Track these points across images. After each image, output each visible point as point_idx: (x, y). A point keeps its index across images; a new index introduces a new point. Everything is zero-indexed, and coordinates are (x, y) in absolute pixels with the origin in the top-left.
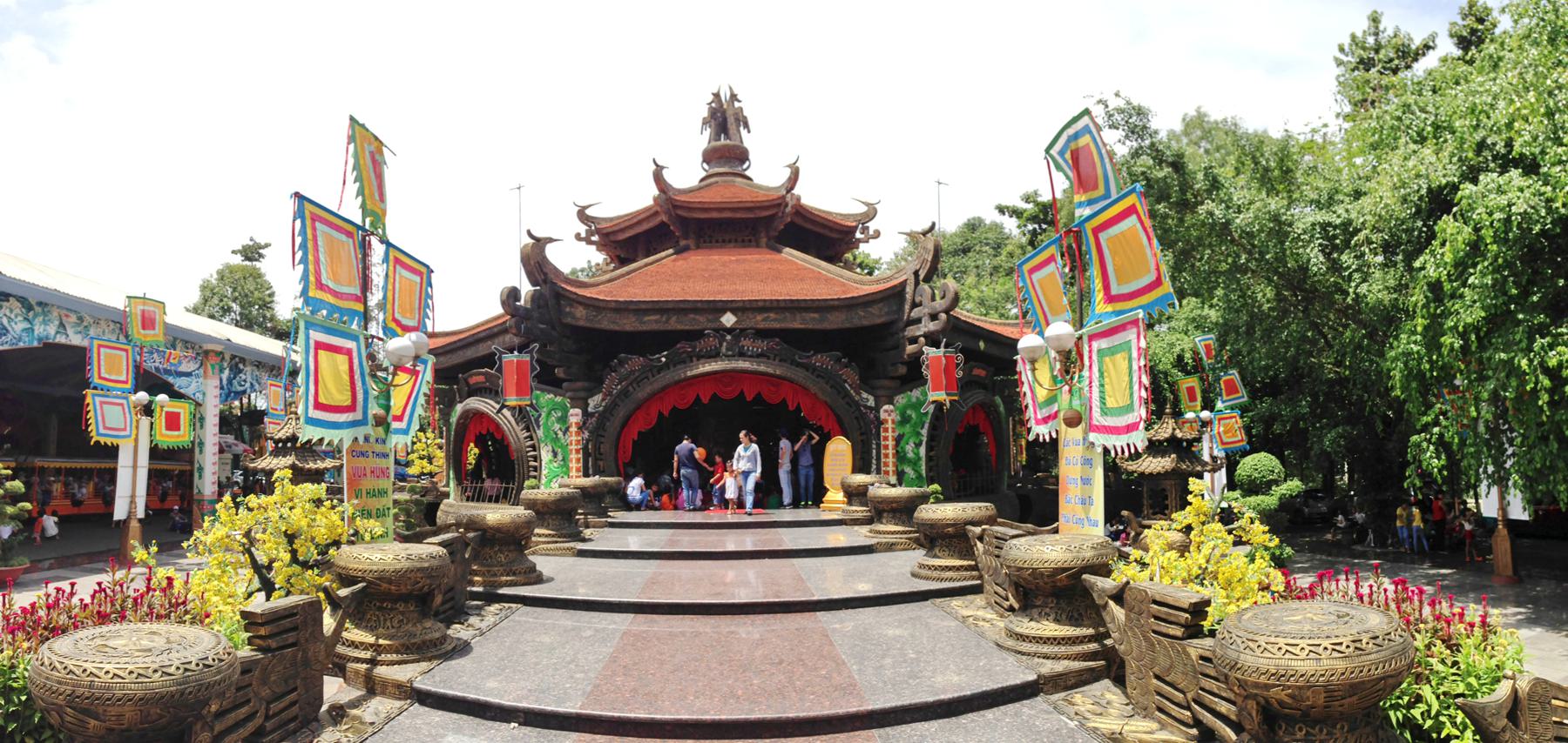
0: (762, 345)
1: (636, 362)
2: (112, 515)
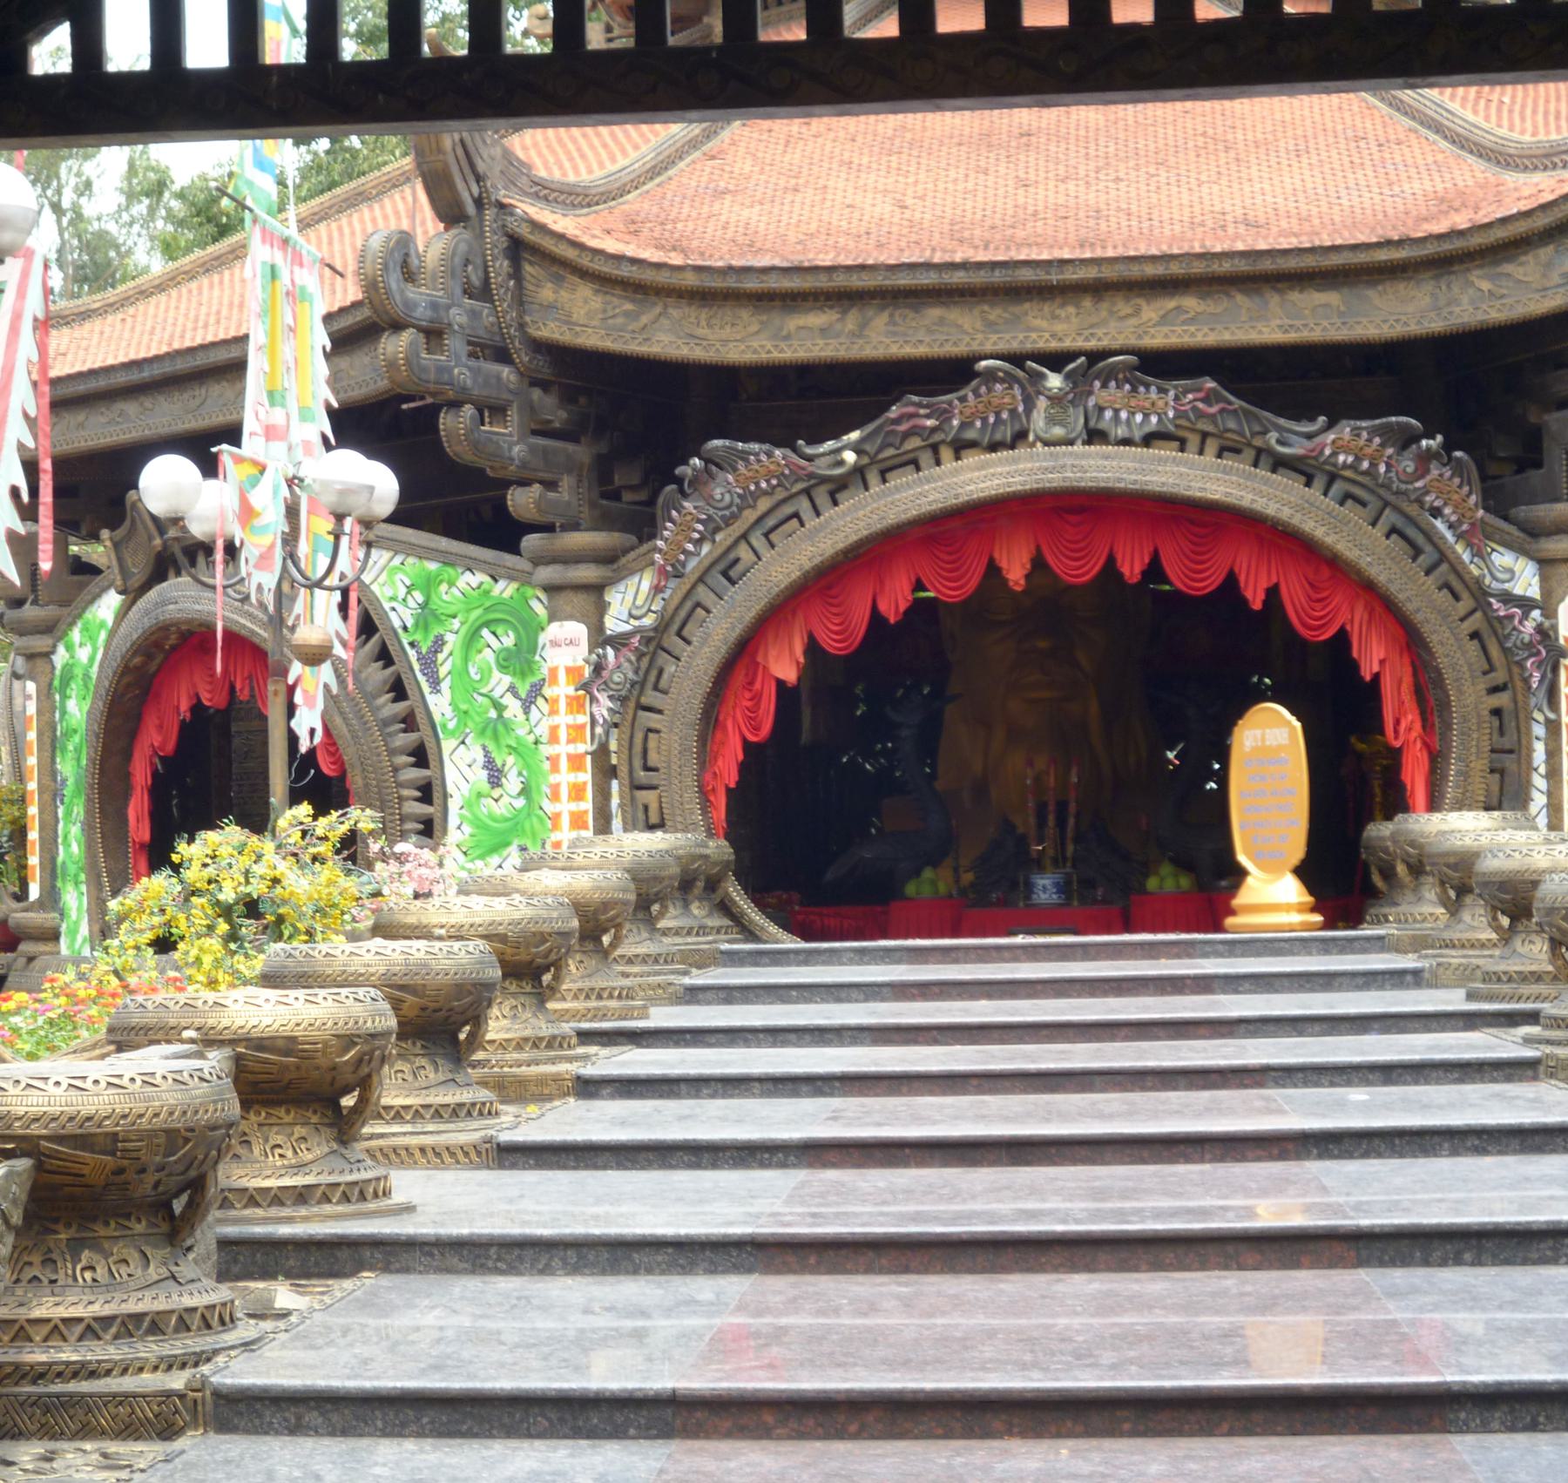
0: (1163, 403)
1: (766, 460)
2: (72, 26)
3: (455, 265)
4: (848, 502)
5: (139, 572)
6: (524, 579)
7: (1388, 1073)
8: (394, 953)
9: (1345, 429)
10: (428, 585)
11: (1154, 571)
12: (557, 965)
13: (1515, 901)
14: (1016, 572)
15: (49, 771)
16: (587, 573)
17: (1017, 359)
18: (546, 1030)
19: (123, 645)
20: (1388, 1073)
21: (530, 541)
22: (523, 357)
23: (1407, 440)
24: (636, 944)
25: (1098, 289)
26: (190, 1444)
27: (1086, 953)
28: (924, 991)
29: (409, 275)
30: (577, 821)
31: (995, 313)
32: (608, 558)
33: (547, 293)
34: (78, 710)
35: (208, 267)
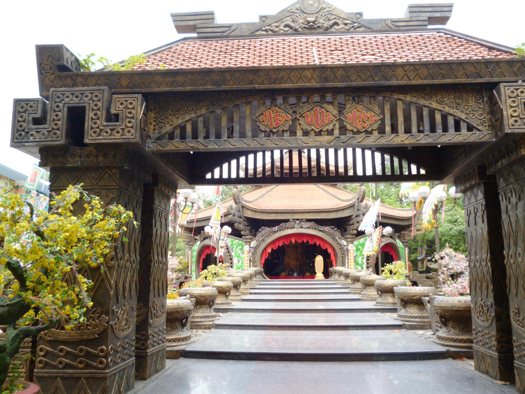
0: (309, 224)
1: (268, 229)
3: (236, 208)
4: (276, 234)
5: (202, 239)
6: (242, 241)
7: (335, 293)
8: (231, 278)
9: (327, 227)
10: (232, 241)
11: (307, 242)
12: (247, 280)
13: (347, 276)
14: (293, 241)
15: (191, 260)
16: (249, 240)
17: (294, 219)
18: (246, 287)
19: (200, 247)
20: (335, 293)
21: (243, 237)
22: (243, 218)
23: (333, 229)
24: (254, 279)
25: (302, 212)
26: (213, 330)
27: (301, 281)
28: (285, 284)
29: (232, 209)
30: (247, 266)
31: (292, 215)
32: (251, 239)
33: (246, 211)
34: (195, 254)
35: (210, 208)
